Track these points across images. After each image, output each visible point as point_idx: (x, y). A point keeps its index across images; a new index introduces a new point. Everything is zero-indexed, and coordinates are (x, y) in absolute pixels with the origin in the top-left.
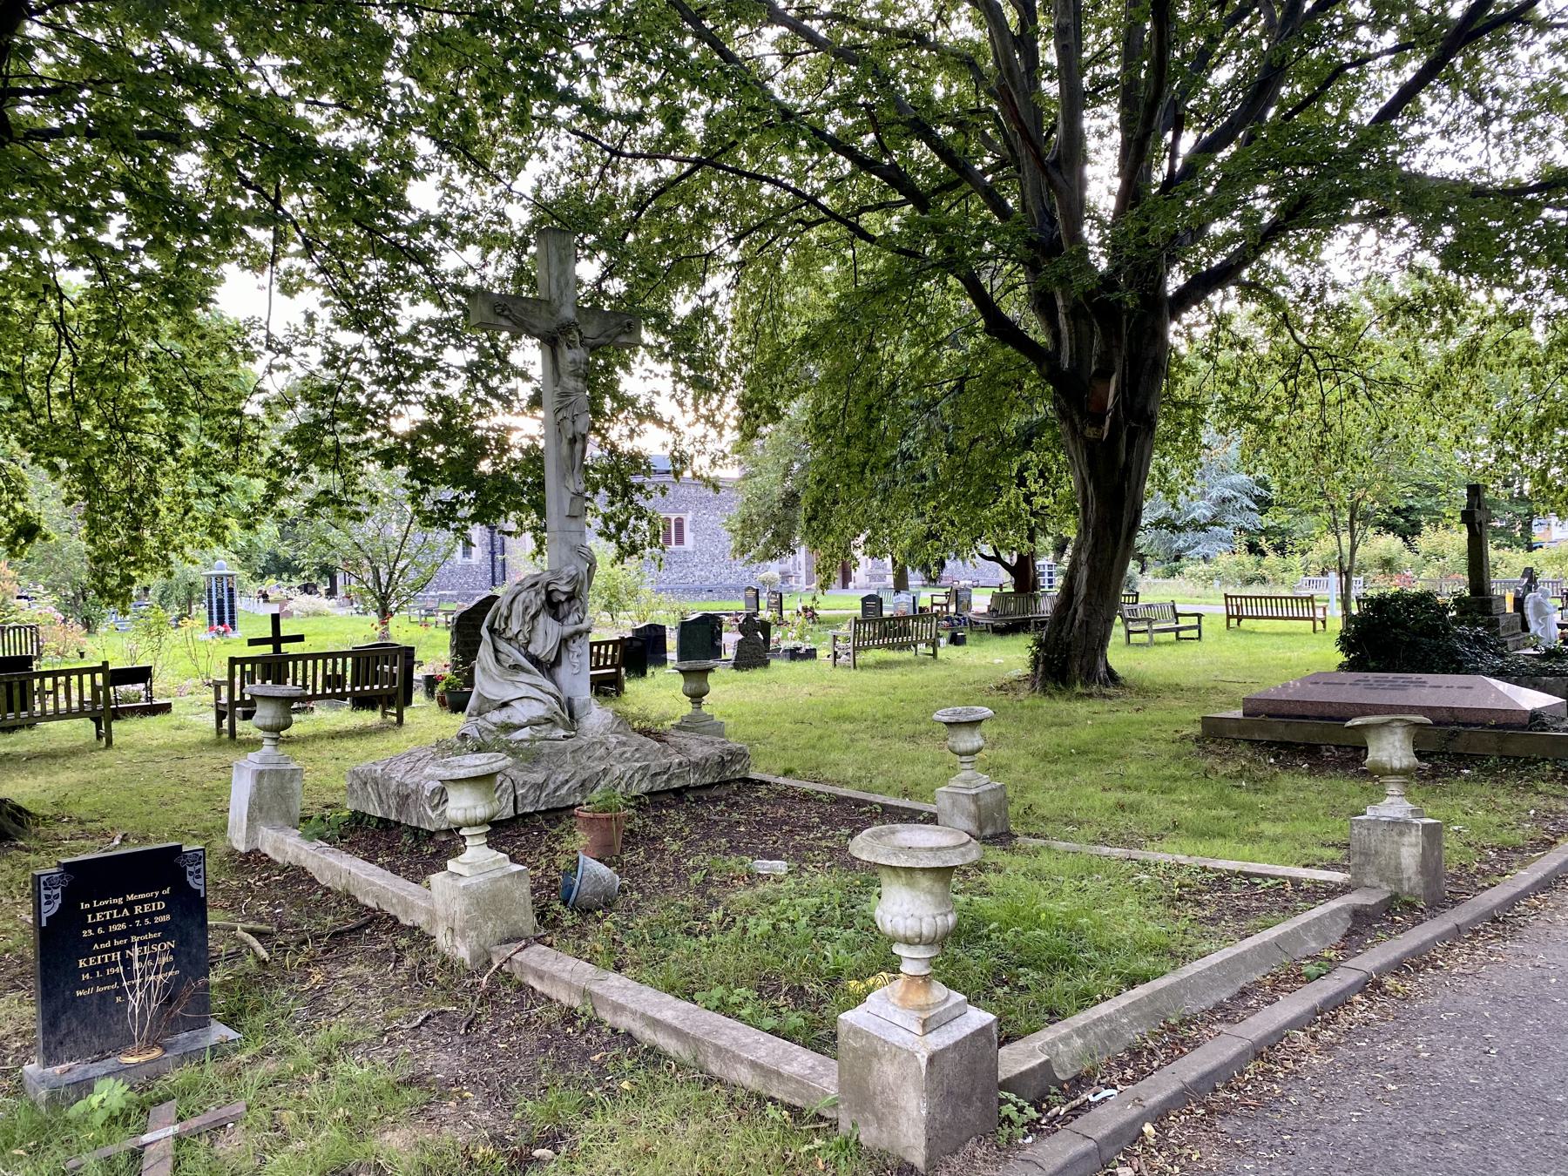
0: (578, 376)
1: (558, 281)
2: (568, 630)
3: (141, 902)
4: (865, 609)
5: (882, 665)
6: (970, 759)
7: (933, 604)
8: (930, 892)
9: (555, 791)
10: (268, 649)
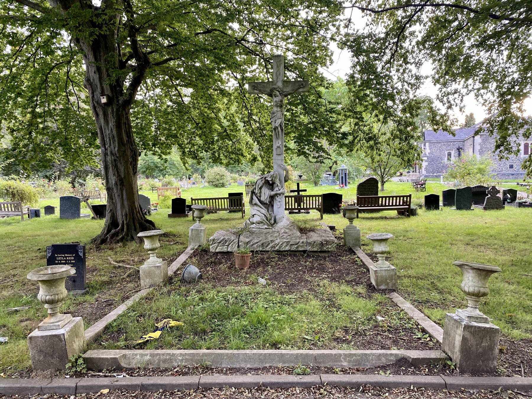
0: (278, 106)
2: (273, 193)
3: (68, 257)
9: (252, 245)
10: (296, 193)
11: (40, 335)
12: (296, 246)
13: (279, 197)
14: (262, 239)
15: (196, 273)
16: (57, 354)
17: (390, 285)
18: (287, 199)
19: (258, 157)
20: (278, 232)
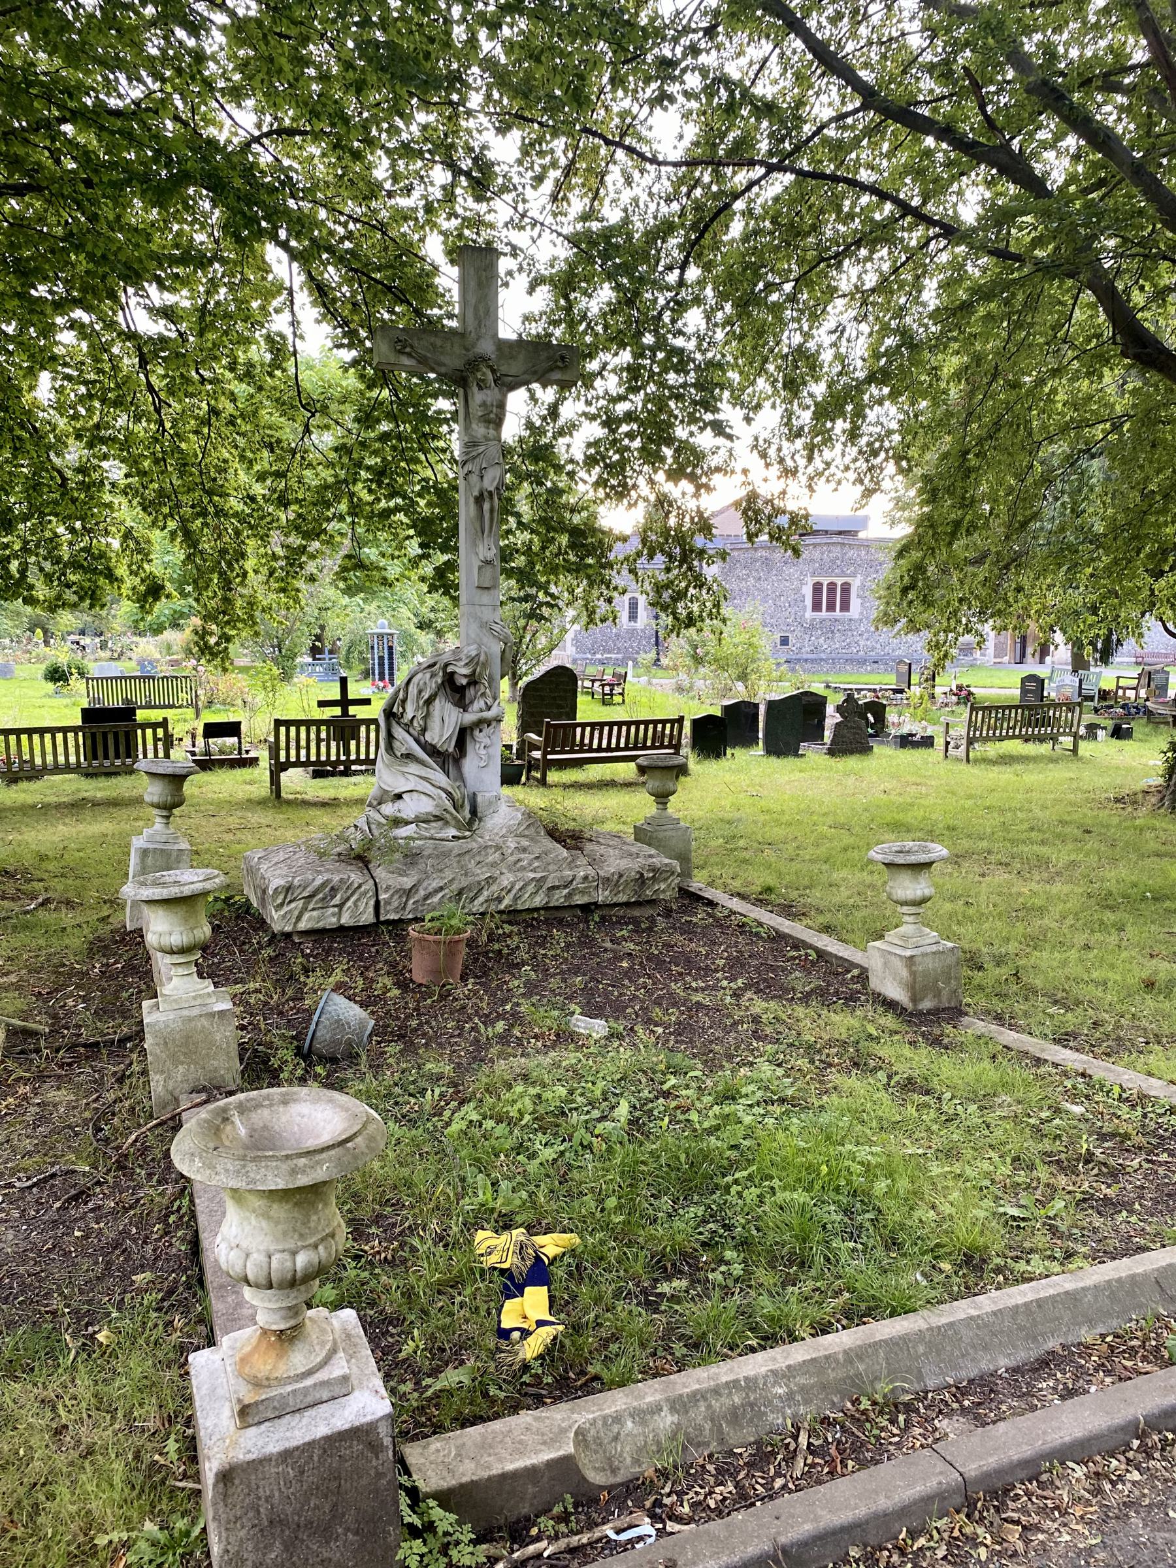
1: (476, 309)
2: (469, 718)
4: (1024, 691)
5: (1005, 760)
6: (914, 910)
7: (1118, 687)
8: (267, 1216)
9: (426, 898)
10: (337, 711)
11: (274, 1448)
12: (565, 891)
13: (486, 731)
14: (449, 876)
15: (362, 1025)
16: (349, 1518)
17: (945, 993)
18: (283, 729)
19: (168, 584)
20: (498, 848)
